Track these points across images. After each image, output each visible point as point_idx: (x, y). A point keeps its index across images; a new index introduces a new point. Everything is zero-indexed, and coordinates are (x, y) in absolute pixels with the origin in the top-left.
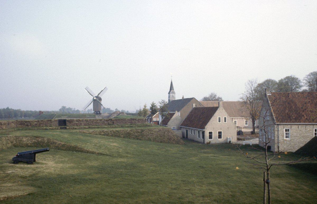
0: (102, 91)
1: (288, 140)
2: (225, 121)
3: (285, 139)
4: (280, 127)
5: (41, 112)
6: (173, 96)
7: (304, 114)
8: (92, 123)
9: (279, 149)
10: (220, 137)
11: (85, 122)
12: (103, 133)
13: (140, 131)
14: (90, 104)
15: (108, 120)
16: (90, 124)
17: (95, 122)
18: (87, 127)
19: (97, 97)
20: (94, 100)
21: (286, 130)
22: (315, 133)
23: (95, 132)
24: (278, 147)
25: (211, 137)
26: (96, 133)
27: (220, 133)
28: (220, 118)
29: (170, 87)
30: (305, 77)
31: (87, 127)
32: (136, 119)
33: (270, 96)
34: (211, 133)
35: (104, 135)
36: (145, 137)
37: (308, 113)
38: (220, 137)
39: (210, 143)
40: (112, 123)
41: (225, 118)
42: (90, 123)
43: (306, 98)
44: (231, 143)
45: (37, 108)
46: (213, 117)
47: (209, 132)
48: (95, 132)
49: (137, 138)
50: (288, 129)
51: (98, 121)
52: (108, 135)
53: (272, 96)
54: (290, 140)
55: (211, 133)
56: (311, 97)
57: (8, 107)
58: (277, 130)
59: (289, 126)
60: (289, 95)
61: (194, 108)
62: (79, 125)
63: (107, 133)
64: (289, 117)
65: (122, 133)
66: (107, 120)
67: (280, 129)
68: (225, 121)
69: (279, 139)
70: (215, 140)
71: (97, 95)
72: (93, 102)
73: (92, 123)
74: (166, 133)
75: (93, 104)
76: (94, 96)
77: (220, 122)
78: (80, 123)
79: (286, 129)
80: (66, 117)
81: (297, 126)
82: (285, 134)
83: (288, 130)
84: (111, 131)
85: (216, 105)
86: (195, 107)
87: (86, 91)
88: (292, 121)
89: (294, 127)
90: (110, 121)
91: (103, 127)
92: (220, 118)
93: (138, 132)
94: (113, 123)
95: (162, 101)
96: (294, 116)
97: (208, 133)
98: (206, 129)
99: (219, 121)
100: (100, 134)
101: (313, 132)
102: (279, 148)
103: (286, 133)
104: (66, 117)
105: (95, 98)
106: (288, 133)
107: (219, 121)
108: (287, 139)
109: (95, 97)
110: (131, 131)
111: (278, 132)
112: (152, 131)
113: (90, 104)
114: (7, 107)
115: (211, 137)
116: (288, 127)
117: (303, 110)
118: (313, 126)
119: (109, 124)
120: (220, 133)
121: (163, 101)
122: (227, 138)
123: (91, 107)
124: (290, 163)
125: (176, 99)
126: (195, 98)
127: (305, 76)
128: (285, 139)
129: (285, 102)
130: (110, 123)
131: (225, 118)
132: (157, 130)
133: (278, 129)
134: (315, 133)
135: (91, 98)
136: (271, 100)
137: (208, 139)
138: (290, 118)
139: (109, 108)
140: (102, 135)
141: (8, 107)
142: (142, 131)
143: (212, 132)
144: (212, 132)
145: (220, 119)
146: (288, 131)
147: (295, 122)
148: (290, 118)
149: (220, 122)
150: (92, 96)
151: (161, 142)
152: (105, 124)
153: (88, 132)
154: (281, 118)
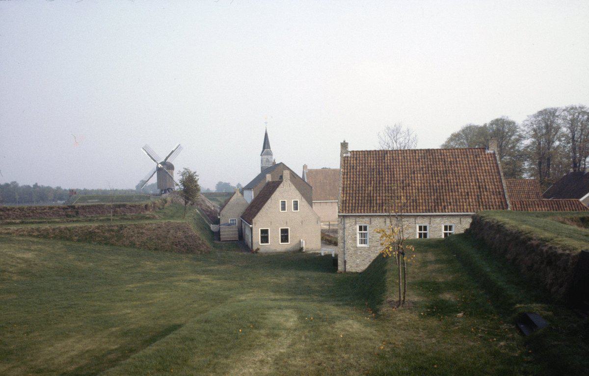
0: (173, 152)
1: (365, 247)
2: (296, 208)
3: (359, 245)
4: (347, 221)
5: (73, 190)
7: (402, 194)
8: (31, 214)
9: (347, 266)
10: (285, 238)
11: (17, 211)
12: (36, 234)
13: (116, 228)
14: (151, 177)
15: (67, 208)
16: (27, 217)
17: (39, 211)
18: (18, 221)
19: (163, 163)
20: (159, 170)
21: (446, 228)
22: (419, 233)
23: (20, 232)
24: (345, 262)
25: (265, 239)
26: (22, 233)
27: (285, 232)
28: (285, 201)
29: (263, 142)
30: (525, 119)
31: (18, 221)
32: (124, 206)
33: (347, 157)
34: (265, 233)
35: (37, 237)
36: (125, 239)
37: (411, 191)
38: (285, 238)
39: (258, 251)
40: (74, 214)
41: (296, 203)
42: (27, 215)
43: (419, 161)
44: (304, 251)
45: (67, 184)
46: (269, 201)
47: (261, 230)
48: (20, 232)
49: (106, 242)
50: (365, 225)
51: (45, 211)
52: (45, 237)
53: (351, 157)
54: (369, 248)
55: (265, 233)
56: (430, 159)
57: (36, 184)
58: (343, 227)
59: (367, 219)
60: (386, 156)
61: (269, 182)
62: (6, 218)
63: (45, 234)
65: (76, 232)
66: (64, 209)
67: (347, 225)
68: (296, 208)
69: (346, 246)
70: (275, 245)
71: (163, 160)
72: (157, 173)
73: (31, 214)
74: (172, 231)
75: (156, 178)
76: (159, 162)
77: (297, 209)
78: (8, 214)
79: (360, 225)
80: (97, 200)
81: (382, 220)
82: (358, 236)
83: (365, 228)
84: (54, 230)
86: (270, 180)
87: (144, 152)
88: (373, 210)
90: (69, 210)
91: (53, 220)
92: (285, 201)
93: (113, 231)
94: (77, 213)
95: (184, 170)
96: (379, 200)
97: (280, 231)
98: (254, 225)
99: (283, 208)
100: (30, 236)
101: (415, 231)
102: (347, 263)
103: (362, 233)
104: (97, 200)
105: (160, 166)
106: (364, 233)
107: (283, 208)
108: (363, 245)
109: (161, 163)
110: (98, 228)
111: (344, 231)
112: (142, 228)
113: (151, 177)
114: (34, 184)
115: (265, 239)
116: (364, 222)
117: (403, 187)
118: (384, 219)
119: (67, 216)
120: (285, 232)
121: (186, 169)
123: (154, 180)
124: (290, 297)
126: (283, 164)
127: (525, 118)
128: (359, 245)
129: (374, 169)
130: (70, 213)
131: (296, 203)
132: (154, 226)
133: (344, 224)
134: (419, 233)
135: (153, 166)
136: (346, 165)
137: (258, 242)
138: (371, 203)
139: (227, 182)
140: (34, 236)
141: (36, 184)
142: (121, 228)
143: (268, 230)
144: (268, 230)
145: (297, 204)
146: (450, 230)
147: (444, 211)
148: (371, 203)
149: (297, 209)
150: (155, 161)
151: (156, 249)
152: (60, 216)
153: (6, 231)
154: (352, 204)
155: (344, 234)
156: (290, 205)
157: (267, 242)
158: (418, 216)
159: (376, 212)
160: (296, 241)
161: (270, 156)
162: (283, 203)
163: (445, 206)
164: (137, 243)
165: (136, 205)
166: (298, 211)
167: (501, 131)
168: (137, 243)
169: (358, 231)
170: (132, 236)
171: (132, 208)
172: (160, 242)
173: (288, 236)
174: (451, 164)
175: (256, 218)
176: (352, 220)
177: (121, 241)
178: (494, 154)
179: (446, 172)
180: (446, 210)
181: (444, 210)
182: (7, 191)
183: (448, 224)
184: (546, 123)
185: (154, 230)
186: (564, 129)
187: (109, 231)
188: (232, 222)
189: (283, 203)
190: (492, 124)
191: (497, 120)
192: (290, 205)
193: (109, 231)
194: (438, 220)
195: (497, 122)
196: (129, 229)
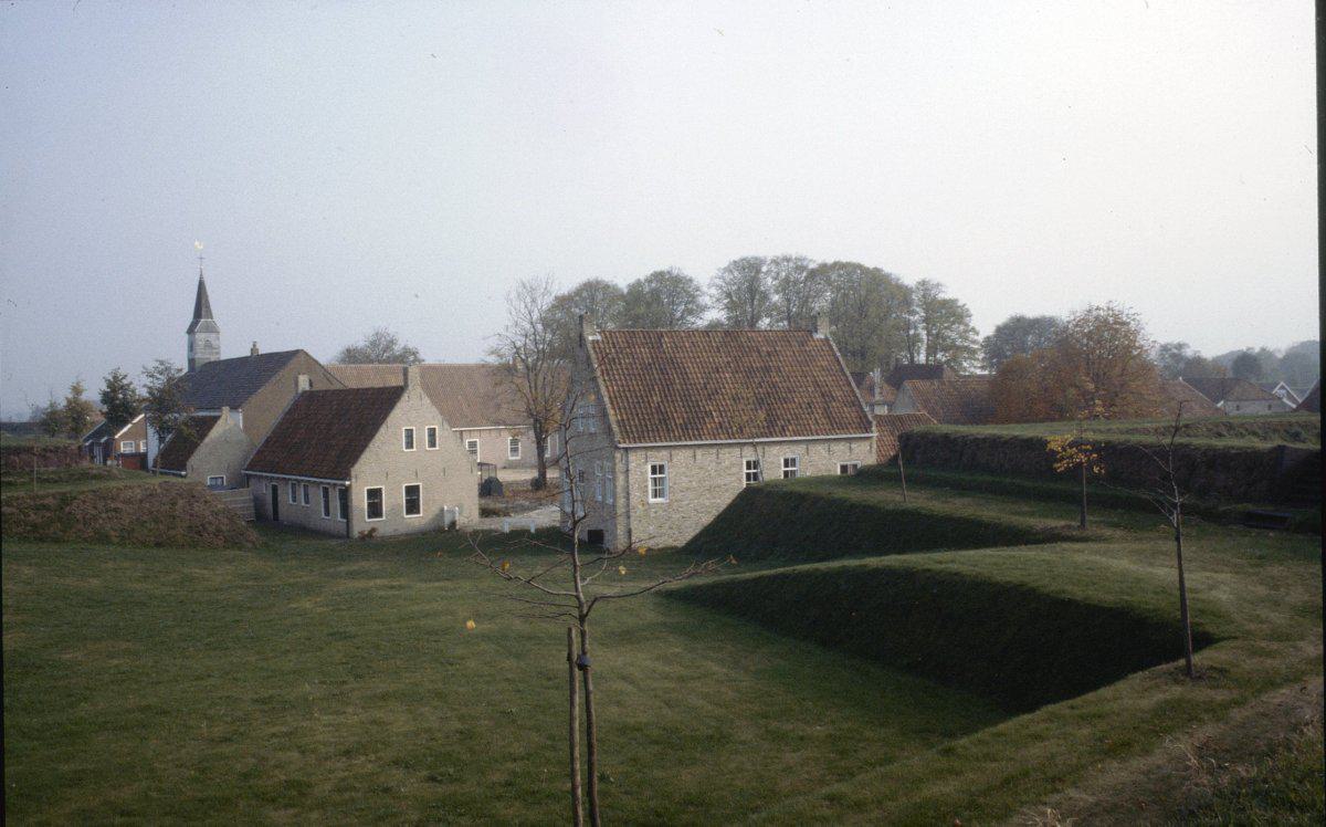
1: (662, 504)
2: (432, 444)
6: (208, 345)
10: (413, 506)
13: (50, 501)
25: (375, 510)
27: (412, 492)
33: (598, 341)
34: (374, 494)
36: (81, 526)
38: (413, 506)
41: (432, 433)
44: (457, 527)
46: (383, 430)
54: (669, 505)
55: (374, 494)
59: (665, 453)
64: (665, 421)
68: (432, 444)
70: (395, 520)
77: (412, 447)
82: (650, 483)
85: (394, 381)
86: (307, 388)
89: (682, 456)
98: (353, 480)
99: (410, 444)
101: (741, 469)
107: (410, 444)
108: (659, 500)
115: (375, 510)
116: (659, 458)
120: (412, 492)
121: (162, 363)
122: (442, 510)
125: (224, 356)
127: (714, 273)
129: (650, 365)
131: (432, 433)
143: (380, 490)
144: (380, 490)
149: (412, 447)
151: (158, 545)
155: (627, 482)
156: (422, 436)
157: (380, 515)
158: (745, 444)
159: (681, 440)
160: (435, 510)
161: (214, 335)
162: (409, 434)
163: (783, 427)
164: (113, 533)
165: (58, 448)
166: (415, 449)
167: (667, 290)
168: (113, 533)
169: (650, 475)
170: (95, 518)
171: (48, 454)
172: (161, 527)
173: (418, 499)
174: (769, 356)
175: (357, 466)
176: (641, 454)
177: (74, 530)
178: (827, 339)
179: (767, 370)
180: (787, 433)
181: (783, 432)
182: (5, 419)
183: (790, 456)
184: (746, 282)
185: (141, 501)
186: (776, 298)
187: (37, 509)
188: (214, 483)
189: (409, 434)
190: (649, 281)
191: (661, 274)
192: (422, 436)
193: (37, 509)
194: (775, 450)
195: (659, 277)
196: (84, 502)
